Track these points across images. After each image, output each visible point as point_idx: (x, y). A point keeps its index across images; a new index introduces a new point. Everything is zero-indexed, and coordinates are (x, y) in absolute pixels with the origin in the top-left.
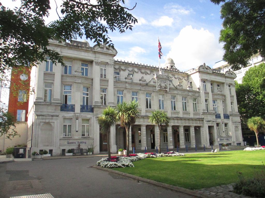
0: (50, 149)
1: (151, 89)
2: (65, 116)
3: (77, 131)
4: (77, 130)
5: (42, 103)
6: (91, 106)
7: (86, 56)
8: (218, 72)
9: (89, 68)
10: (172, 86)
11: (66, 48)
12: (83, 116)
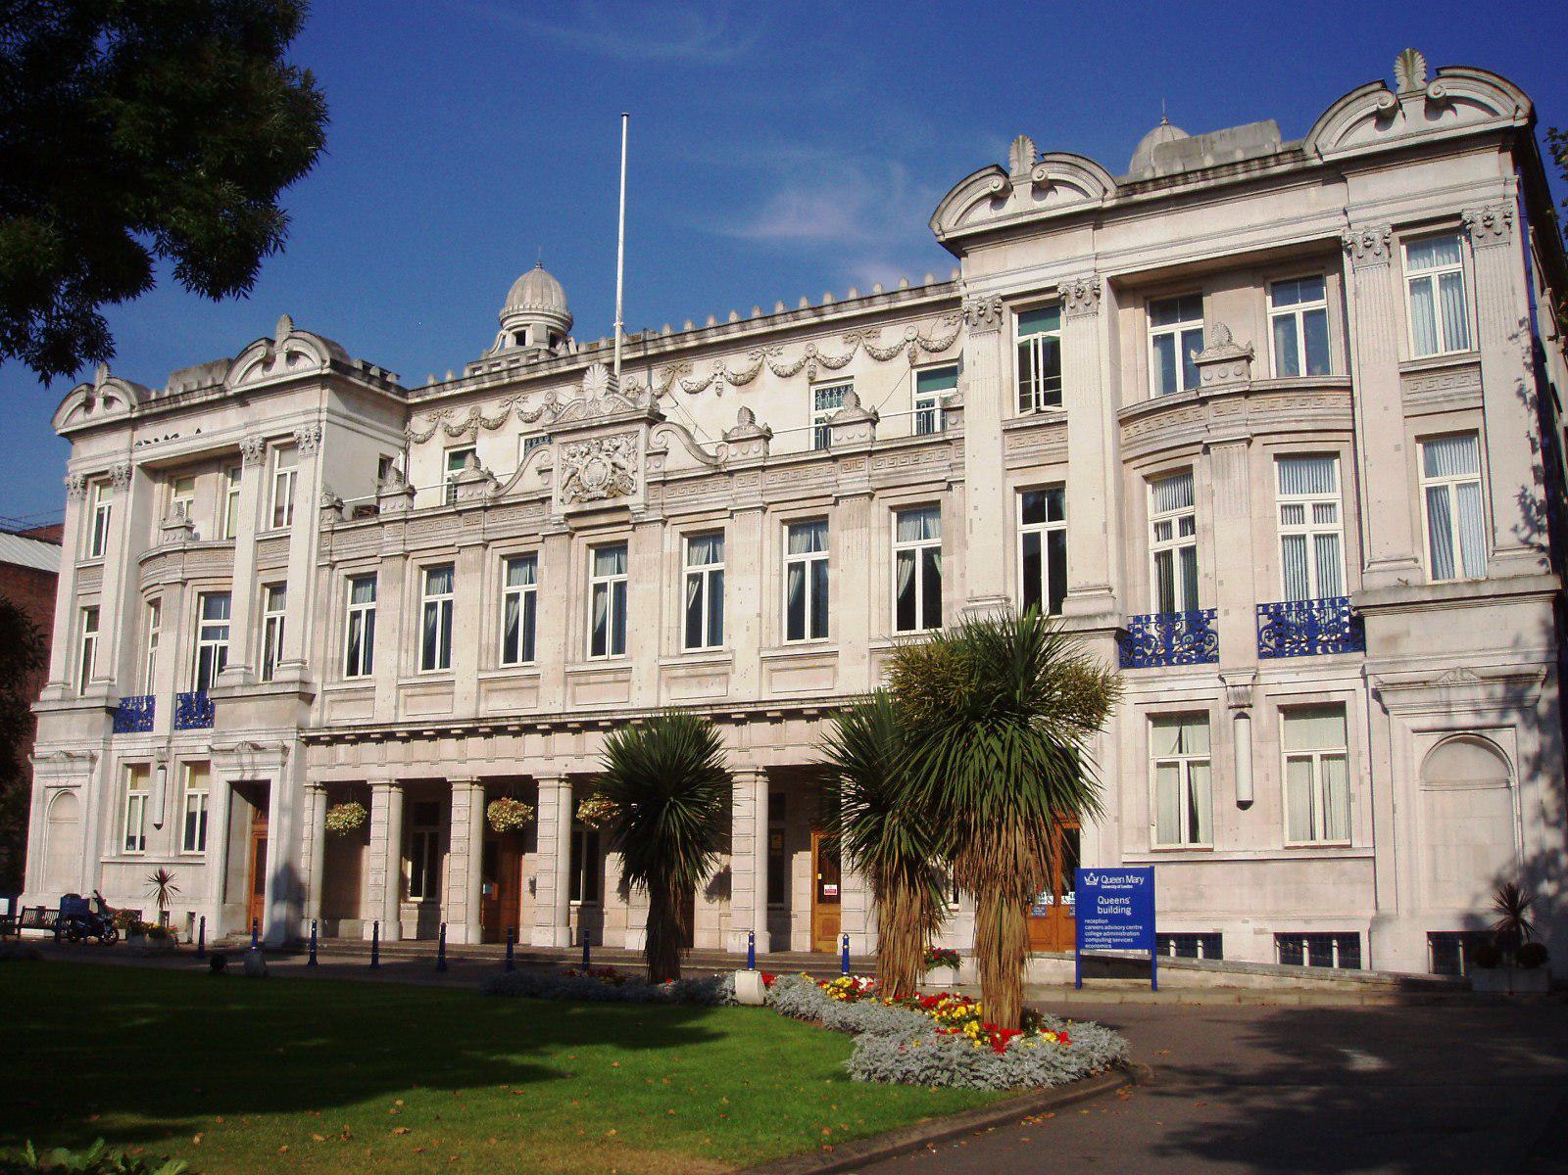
0: (1224, 938)
1: (526, 519)
2: (128, 753)
3: (1244, 805)
4: (1245, 797)
5: (237, 693)
7: (1299, 220)
8: (167, 393)
9: (1327, 301)
10: (680, 460)
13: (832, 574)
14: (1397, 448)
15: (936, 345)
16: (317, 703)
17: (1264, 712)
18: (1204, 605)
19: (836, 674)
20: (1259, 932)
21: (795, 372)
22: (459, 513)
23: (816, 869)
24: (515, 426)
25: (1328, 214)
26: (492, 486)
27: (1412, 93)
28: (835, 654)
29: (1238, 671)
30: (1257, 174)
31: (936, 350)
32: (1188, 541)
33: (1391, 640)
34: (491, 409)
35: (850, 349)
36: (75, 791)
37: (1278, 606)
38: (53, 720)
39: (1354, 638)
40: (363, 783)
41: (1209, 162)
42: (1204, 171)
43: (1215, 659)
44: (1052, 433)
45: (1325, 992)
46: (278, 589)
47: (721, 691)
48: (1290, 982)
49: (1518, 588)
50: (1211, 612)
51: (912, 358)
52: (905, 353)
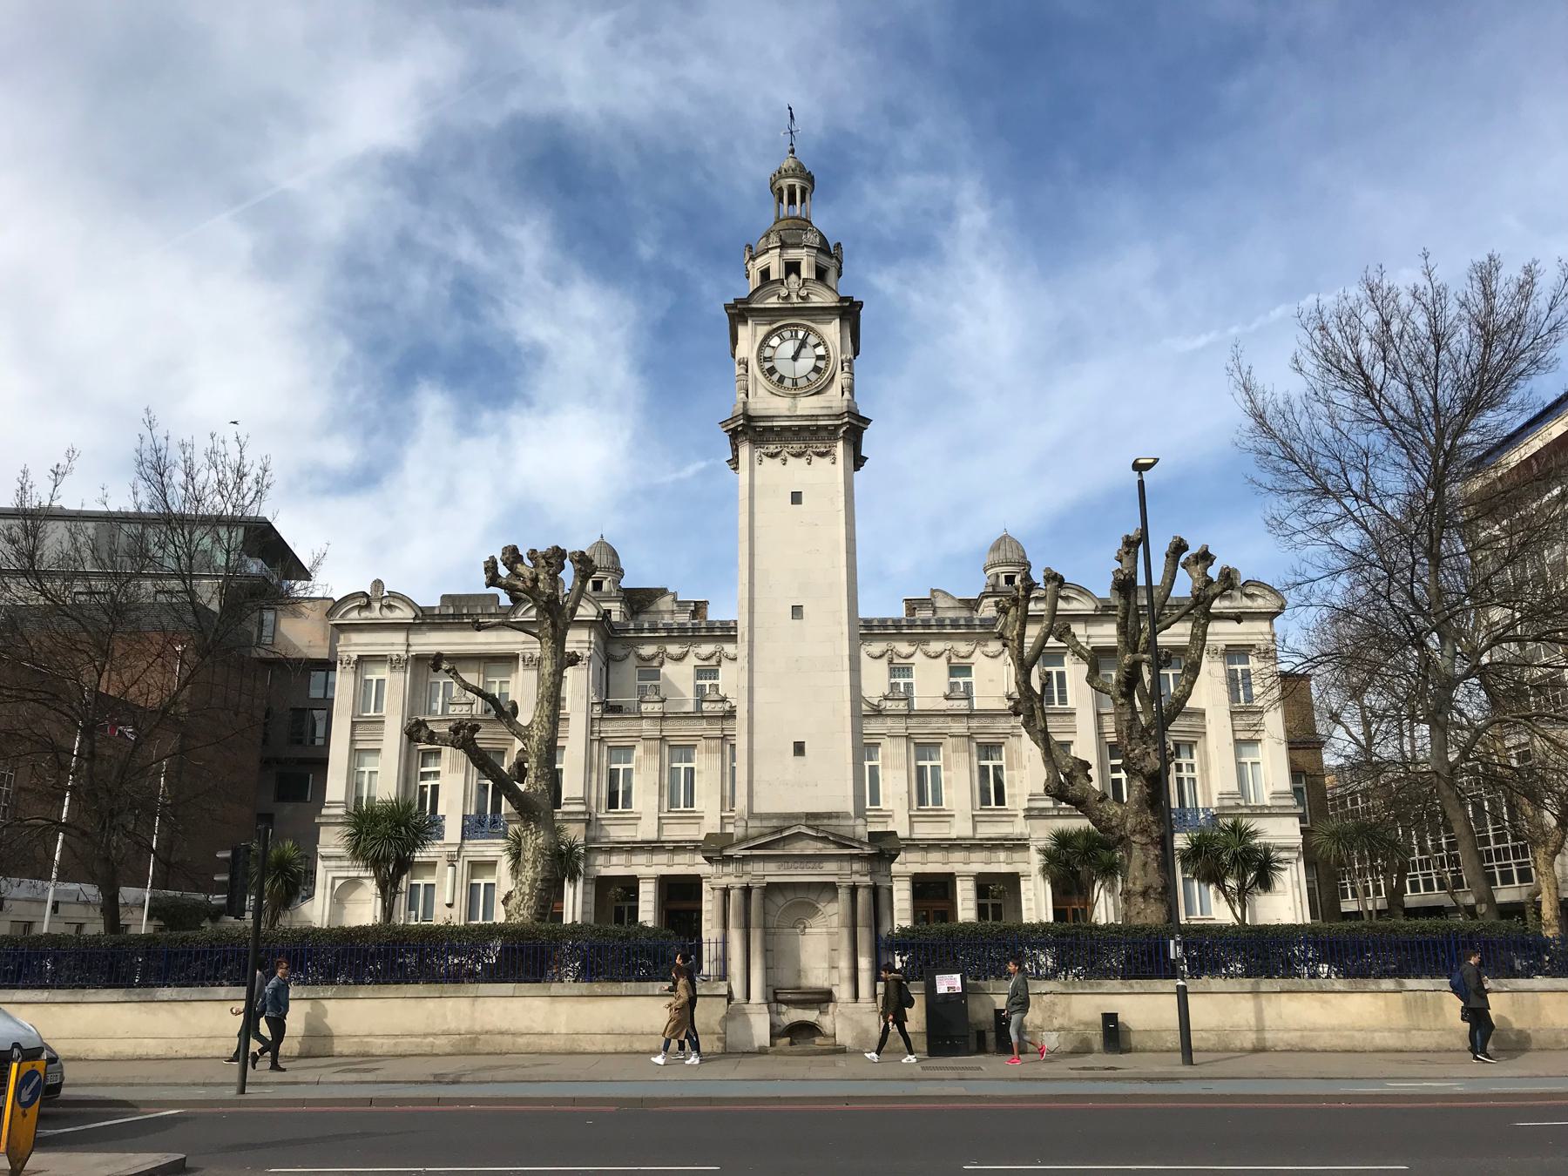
6: (1208, 809)
11: (424, 627)
12: (471, 854)
14: (1376, 323)
15: (963, 654)
18: (440, 813)
21: (881, 657)
22: (704, 717)
24: (692, 661)
26: (728, 705)
28: (953, 816)
31: (963, 657)
34: (674, 649)
35: (913, 649)
51: (949, 660)
52: (944, 656)
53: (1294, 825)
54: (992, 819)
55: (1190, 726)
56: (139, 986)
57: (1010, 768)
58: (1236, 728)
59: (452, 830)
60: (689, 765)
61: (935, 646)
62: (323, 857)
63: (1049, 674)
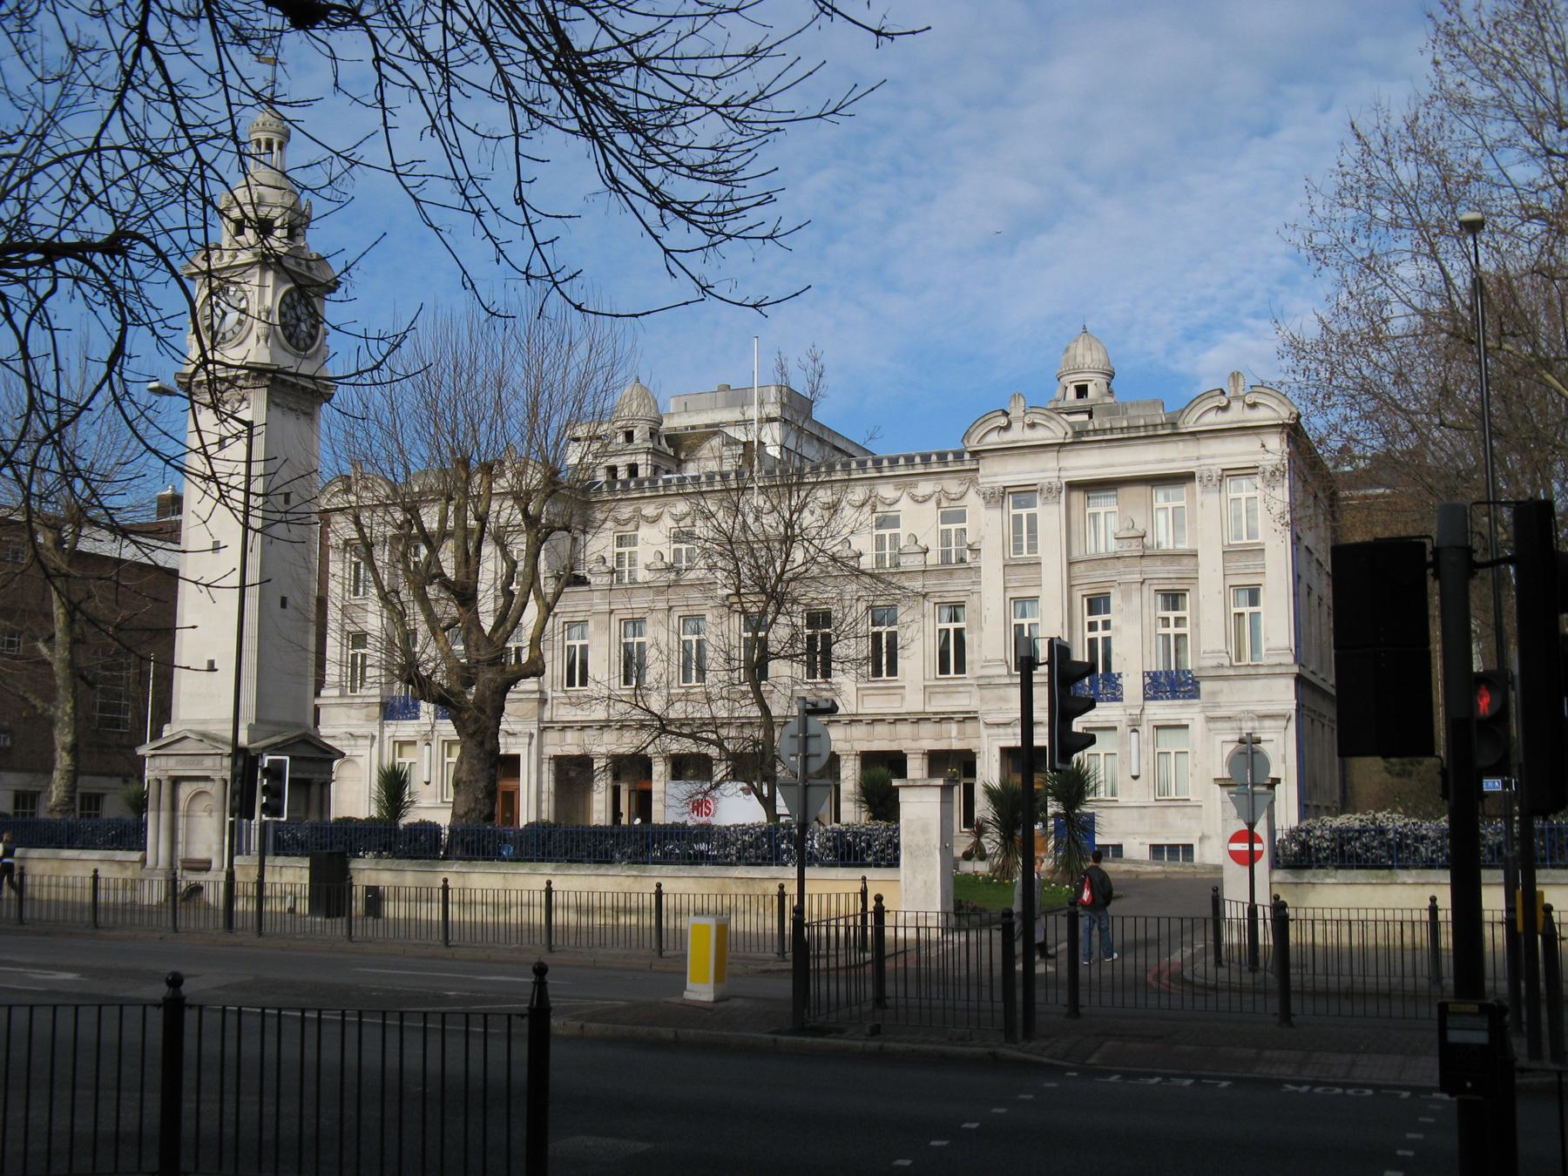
3: (1135, 778)
7: (1173, 460)
13: (967, 637)
16: (548, 706)
17: (1146, 730)
18: (1115, 670)
19: (903, 699)
20: (1141, 844)
21: (863, 505)
23: (633, 810)
24: (668, 522)
25: (1190, 459)
27: (1237, 398)
28: (904, 687)
29: (1132, 707)
30: (1151, 433)
32: (1107, 633)
33: (1214, 694)
35: (898, 494)
36: (357, 759)
37: (1155, 673)
38: (334, 710)
39: (1194, 693)
40: (900, 752)
41: (1125, 424)
42: (1122, 429)
43: (1121, 700)
44: (1032, 569)
45: (1175, 872)
46: (1254, 596)
47: (966, 702)
48: (1158, 868)
49: (1278, 670)
50: (1119, 675)
51: (939, 503)
52: (934, 500)
53: (1288, 687)
54: (948, 692)
55: (1022, 580)
56: (444, 858)
57: (971, 632)
58: (1008, 585)
59: (1132, 685)
60: (958, 625)
61: (925, 487)
62: (986, 724)
63: (680, 550)
